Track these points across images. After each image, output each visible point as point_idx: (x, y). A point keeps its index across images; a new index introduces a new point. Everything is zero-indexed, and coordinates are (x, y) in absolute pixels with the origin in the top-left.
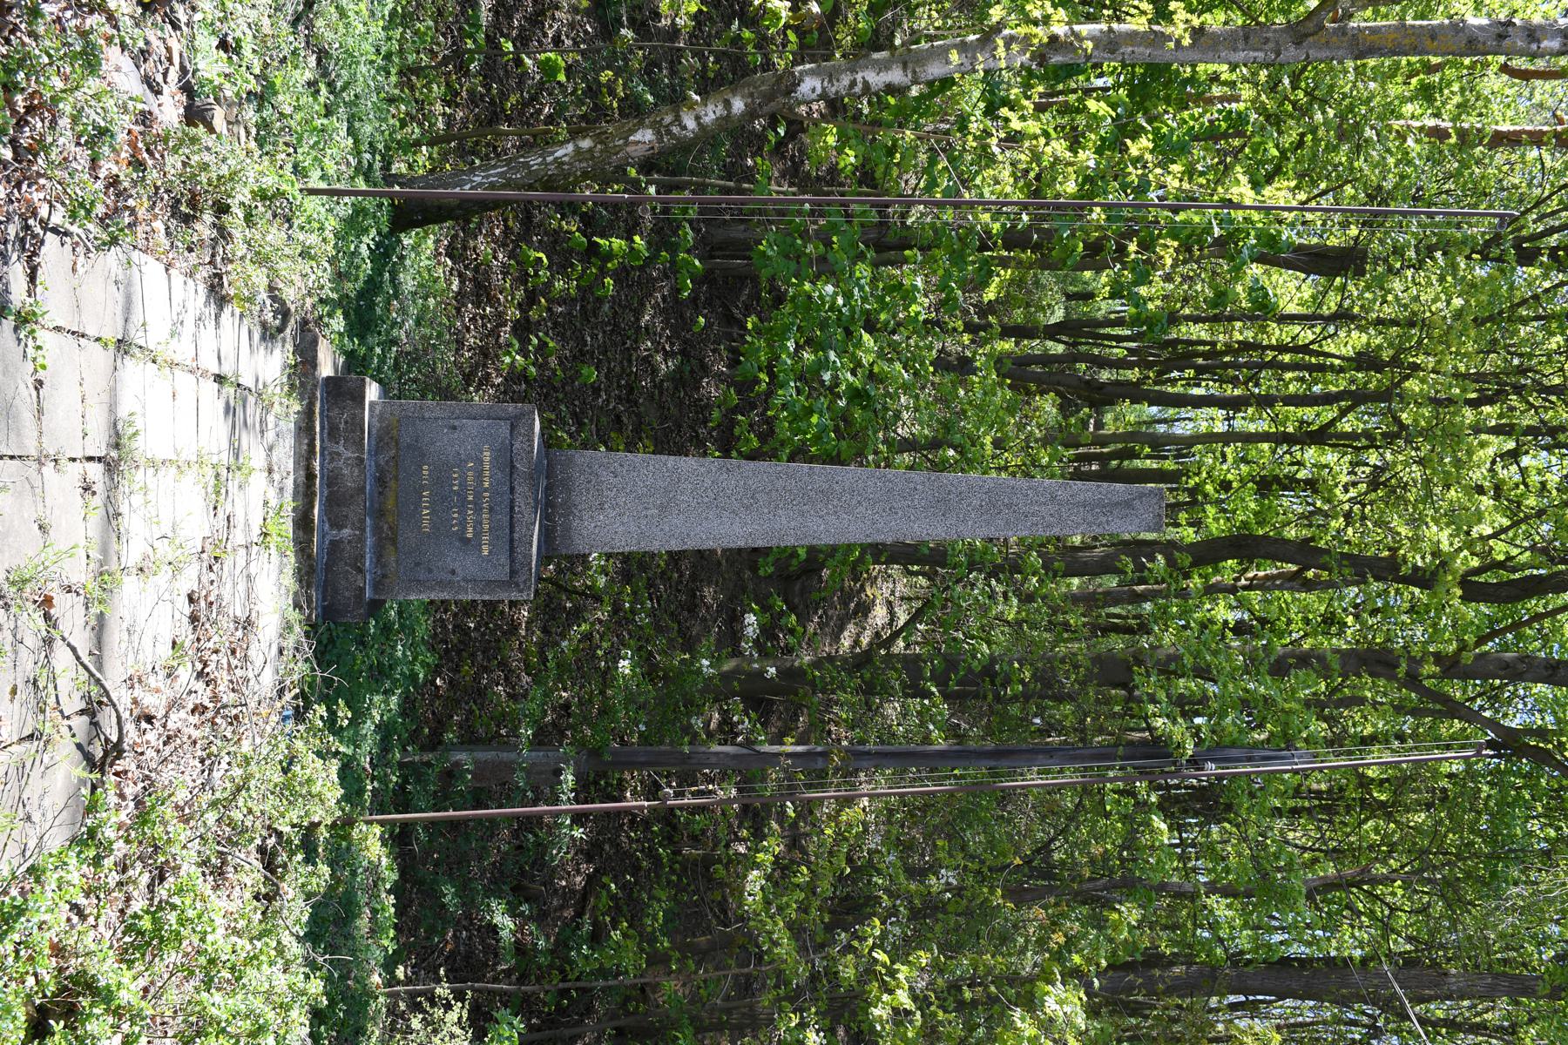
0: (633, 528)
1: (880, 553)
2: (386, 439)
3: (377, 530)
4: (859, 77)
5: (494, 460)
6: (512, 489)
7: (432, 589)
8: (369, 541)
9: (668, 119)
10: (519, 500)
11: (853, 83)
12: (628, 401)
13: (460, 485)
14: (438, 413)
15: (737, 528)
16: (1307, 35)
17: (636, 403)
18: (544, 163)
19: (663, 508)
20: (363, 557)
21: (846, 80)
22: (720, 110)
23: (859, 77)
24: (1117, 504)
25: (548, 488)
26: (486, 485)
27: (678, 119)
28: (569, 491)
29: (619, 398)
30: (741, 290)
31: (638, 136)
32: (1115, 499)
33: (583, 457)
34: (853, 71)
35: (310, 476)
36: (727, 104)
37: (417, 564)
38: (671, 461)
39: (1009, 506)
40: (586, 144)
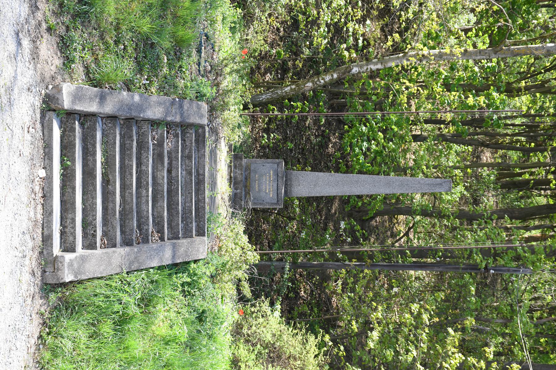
0: (307, 190)
3: (245, 190)
4: (369, 67)
5: (273, 173)
8: (243, 193)
9: (316, 80)
10: (279, 183)
11: (367, 69)
12: (302, 154)
14: (260, 162)
15: (334, 190)
16: (498, 51)
17: (305, 154)
18: (282, 92)
19: (315, 185)
21: (365, 68)
22: (330, 77)
23: (369, 67)
24: (438, 184)
25: (286, 180)
27: (319, 80)
28: (291, 181)
29: (299, 153)
31: (307, 85)
32: (437, 183)
33: (295, 172)
34: (367, 65)
35: (231, 177)
36: (332, 76)
38: (317, 173)
39: (407, 185)
40: (293, 87)
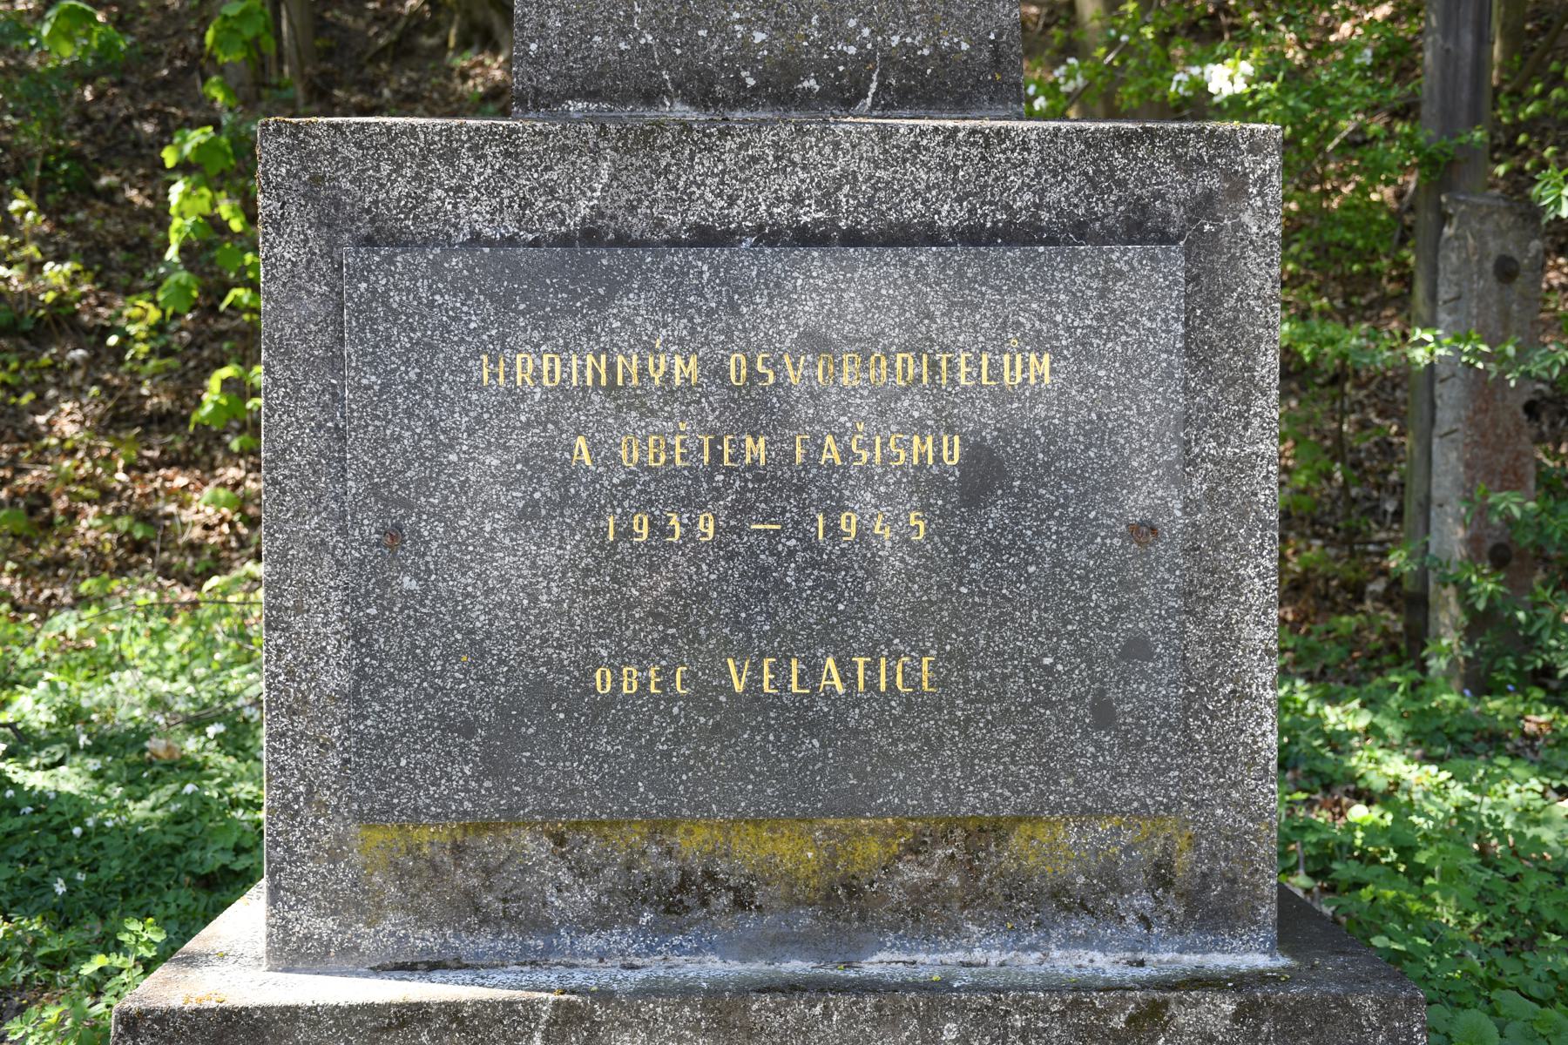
1: (803, 101)
2: (465, 878)
6: (706, 237)
7: (1224, 639)
13: (690, 503)
20: (1079, 992)
26: (685, 369)
30: (345, 30)
37: (1104, 714)
